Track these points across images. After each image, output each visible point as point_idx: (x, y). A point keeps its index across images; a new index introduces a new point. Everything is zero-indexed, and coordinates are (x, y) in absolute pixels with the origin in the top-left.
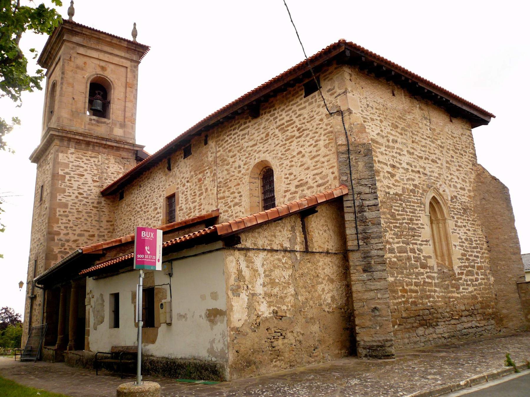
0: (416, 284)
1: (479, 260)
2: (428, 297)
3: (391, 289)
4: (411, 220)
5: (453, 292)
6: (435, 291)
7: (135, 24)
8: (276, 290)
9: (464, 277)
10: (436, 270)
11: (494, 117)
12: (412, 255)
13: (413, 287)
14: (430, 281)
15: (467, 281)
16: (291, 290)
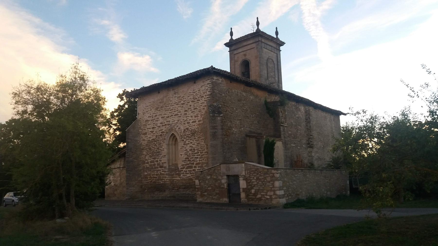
0: (157, 175)
1: (198, 159)
2: (163, 179)
3: (146, 177)
4: (158, 148)
5: (176, 177)
6: (166, 177)
7: (277, 28)
8: (115, 179)
9: (184, 169)
10: (167, 168)
11: (120, 101)
12: (156, 163)
13: (155, 176)
14: (163, 173)
15: (186, 171)
16: (119, 179)
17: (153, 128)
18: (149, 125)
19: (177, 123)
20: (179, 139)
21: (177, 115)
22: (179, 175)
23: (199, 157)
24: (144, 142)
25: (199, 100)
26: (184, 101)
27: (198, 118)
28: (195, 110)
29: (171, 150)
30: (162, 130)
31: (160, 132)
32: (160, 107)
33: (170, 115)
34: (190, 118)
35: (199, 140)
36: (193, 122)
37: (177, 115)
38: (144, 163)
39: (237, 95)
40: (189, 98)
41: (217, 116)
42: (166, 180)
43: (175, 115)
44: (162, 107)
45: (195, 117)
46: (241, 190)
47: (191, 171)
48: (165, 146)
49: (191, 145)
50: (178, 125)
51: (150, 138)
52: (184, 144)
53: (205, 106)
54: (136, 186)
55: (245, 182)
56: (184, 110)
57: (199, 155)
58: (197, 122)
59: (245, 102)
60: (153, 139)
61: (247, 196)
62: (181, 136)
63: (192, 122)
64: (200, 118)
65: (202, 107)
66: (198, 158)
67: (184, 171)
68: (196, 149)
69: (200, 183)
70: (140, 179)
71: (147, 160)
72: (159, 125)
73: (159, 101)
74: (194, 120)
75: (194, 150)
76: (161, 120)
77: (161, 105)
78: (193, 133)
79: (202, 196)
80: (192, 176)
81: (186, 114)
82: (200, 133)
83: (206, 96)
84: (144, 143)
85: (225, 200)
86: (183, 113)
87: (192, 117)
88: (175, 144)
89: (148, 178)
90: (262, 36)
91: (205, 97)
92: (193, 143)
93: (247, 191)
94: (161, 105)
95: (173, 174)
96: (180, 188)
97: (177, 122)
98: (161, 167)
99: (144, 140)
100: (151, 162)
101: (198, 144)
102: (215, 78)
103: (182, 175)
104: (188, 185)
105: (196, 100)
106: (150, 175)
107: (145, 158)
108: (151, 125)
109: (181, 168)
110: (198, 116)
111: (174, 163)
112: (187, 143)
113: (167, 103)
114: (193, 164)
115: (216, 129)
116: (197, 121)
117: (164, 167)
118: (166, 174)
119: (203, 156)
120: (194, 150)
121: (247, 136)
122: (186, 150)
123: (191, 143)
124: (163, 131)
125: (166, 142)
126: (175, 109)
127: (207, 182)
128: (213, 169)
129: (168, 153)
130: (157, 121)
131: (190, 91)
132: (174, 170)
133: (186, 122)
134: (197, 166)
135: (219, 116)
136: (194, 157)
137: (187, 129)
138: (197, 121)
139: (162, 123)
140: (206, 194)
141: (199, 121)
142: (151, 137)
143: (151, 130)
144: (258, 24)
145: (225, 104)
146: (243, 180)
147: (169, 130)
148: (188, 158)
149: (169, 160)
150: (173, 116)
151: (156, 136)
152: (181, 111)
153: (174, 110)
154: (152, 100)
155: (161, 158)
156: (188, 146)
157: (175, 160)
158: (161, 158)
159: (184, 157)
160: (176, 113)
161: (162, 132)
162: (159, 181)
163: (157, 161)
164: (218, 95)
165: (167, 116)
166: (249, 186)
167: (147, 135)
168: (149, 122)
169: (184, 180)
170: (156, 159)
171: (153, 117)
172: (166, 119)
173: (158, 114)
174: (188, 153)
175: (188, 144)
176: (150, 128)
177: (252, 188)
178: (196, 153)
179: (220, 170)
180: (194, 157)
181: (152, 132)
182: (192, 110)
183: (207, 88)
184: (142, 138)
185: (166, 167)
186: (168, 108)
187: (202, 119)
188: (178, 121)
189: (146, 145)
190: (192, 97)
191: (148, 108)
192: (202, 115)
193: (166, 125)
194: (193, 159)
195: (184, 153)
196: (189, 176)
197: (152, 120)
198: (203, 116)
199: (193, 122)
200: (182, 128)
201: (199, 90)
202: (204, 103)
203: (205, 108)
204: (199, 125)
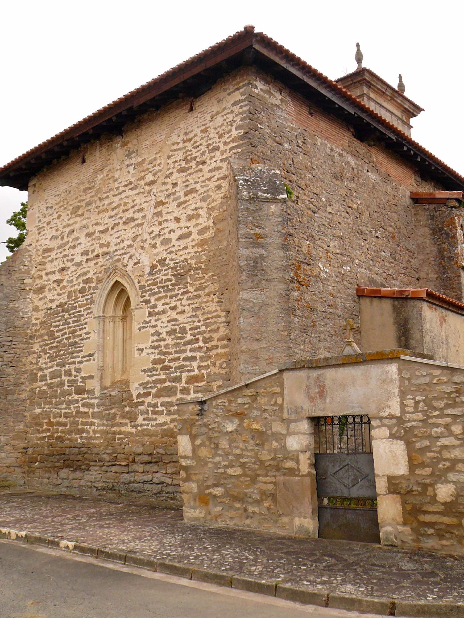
0: (66, 416)
1: (195, 364)
2: (82, 431)
3: (36, 421)
5: (122, 425)
6: (92, 424)
9: (149, 400)
10: (97, 394)
12: (65, 378)
14: (86, 410)
15: (155, 406)
17: (63, 269)
18: (51, 261)
19: (130, 246)
20: (134, 301)
21: (133, 219)
22: (133, 418)
23: (198, 354)
24: (36, 315)
25: (204, 163)
26: (154, 175)
27: (200, 221)
28: (190, 197)
29: (109, 338)
30: (85, 274)
31: (80, 280)
32: (83, 204)
33: (111, 222)
34: (173, 225)
35: (199, 296)
36: (180, 238)
37: (133, 219)
38: (34, 378)
39: (332, 158)
40: (170, 161)
41: (267, 200)
42: (92, 434)
43: (125, 223)
44: (89, 204)
45: (190, 218)
46: (381, 485)
47: (171, 404)
48: (92, 325)
49: (173, 314)
50: (132, 251)
51: (52, 301)
52: (150, 314)
53: (224, 178)
54: (8, 448)
55: (400, 447)
56: (153, 203)
57: (200, 348)
58: (195, 236)
59: (353, 185)
60: (61, 305)
61: (412, 514)
62: (141, 287)
63: (178, 239)
64: (204, 221)
65: (212, 185)
66: (194, 358)
67: (150, 405)
68: (188, 327)
69: (195, 450)
70: (21, 426)
71: (41, 369)
72: (78, 259)
73: (82, 188)
74: (186, 230)
75: (183, 331)
76: (84, 243)
77: (88, 198)
78: (181, 276)
79: (204, 499)
80: (173, 421)
81: (159, 214)
82: (205, 271)
83: (225, 143)
84: (36, 318)
85: (305, 522)
86: (150, 211)
87: (177, 220)
88: (124, 319)
89: (41, 425)
90: (369, 85)
91: (222, 148)
92: (180, 309)
93: (412, 495)
94: (88, 198)
95: (115, 415)
96: (134, 461)
97: (130, 242)
98: (80, 391)
99: (36, 309)
100: (54, 375)
101: (194, 310)
102: (260, 85)
103: (140, 419)
104: (161, 451)
105: (193, 164)
106: (47, 415)
107: (37, 363)
108: (56, 263)
109: (139, 396)
110: (198, 216)
111: (118, 378)
112: (160, 308)
113: (104, 190)
114: (178, 379)
115: (262, 246)
116: (195, 231)
117: (88, 392)
118: (94, 416)
119: (214, 352)
120: (183, 331)
121: (361, 294)
122: (158, 333)
123: (173, 308)
124: (89, 275)
125: (97, 309)
126: (126, 204)
127: (224, 444)
128: (248, 392)
129: (103, 347)
130: (74, 247)
131: (174, 138)
132: (119, 400)
133: (158, 241)
134: (191, 387)
135: (274, 201)
136: (183, 356)
137: (162, 261)
138: (195, 231)
139: (86, 253)
140: (218, 491)
141: (200, 232)
142: (54, 297)
143: (57, 276)
144: (359, 58)
145: (294, 177)
146: (393, 436)
147: (106, 271)
148: (162, 361)
149: (102, 369)
150: (121, 227)
151: (69, 296)
152: (144, 206)
153: (122, 208)
154: (63, 187)
155: (80, 363)
156: (164, 318)
157: (124, 371)
158: (80, 363)
159: (148, 357)
160: (128, 215)
161: (86, 281)
162: (74, 436)
163: (68, 373)
164: (270, 142)
165: (102, 228)
166: (423, 465)
167: (46, 294)
168: (53, 255)
169: (150, 434)
170: (67, 367)
171: (62, 238)
172: (99, 238)
173: (77, 226)
174: (163, 343)
175: (164, 312)
176: (54, 272)
177: (439, 476)
178: (190, 342)
179: (282, 395)
180: (183, 356)
181: (58, 282)
182: (179, 197)
183: (230, 117)
184: (32, 302)
185: (93, 391)
186: (106, 202)
187: (211, 223)
188: (134, 239)
189: (42, 323)
190: (180, 155)
191: (50, 211)
192: (213, 209)
193: (98, 256)
194: (177, 364)
195: (149, 344)
196: (165, 424)
197: (59, 248)
198: (214, 214)
199: (180, 238)
200: (146, 261)
201: (204, 131)
202: (220, 168)
203: (225, 184)
204: (202, 243)
